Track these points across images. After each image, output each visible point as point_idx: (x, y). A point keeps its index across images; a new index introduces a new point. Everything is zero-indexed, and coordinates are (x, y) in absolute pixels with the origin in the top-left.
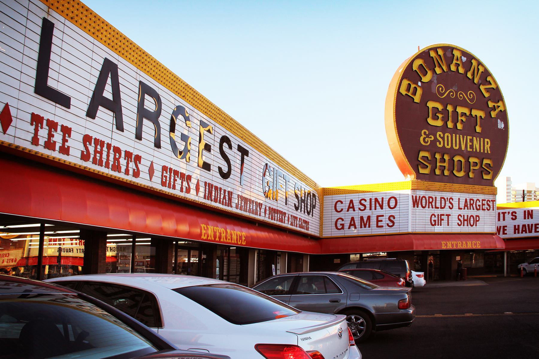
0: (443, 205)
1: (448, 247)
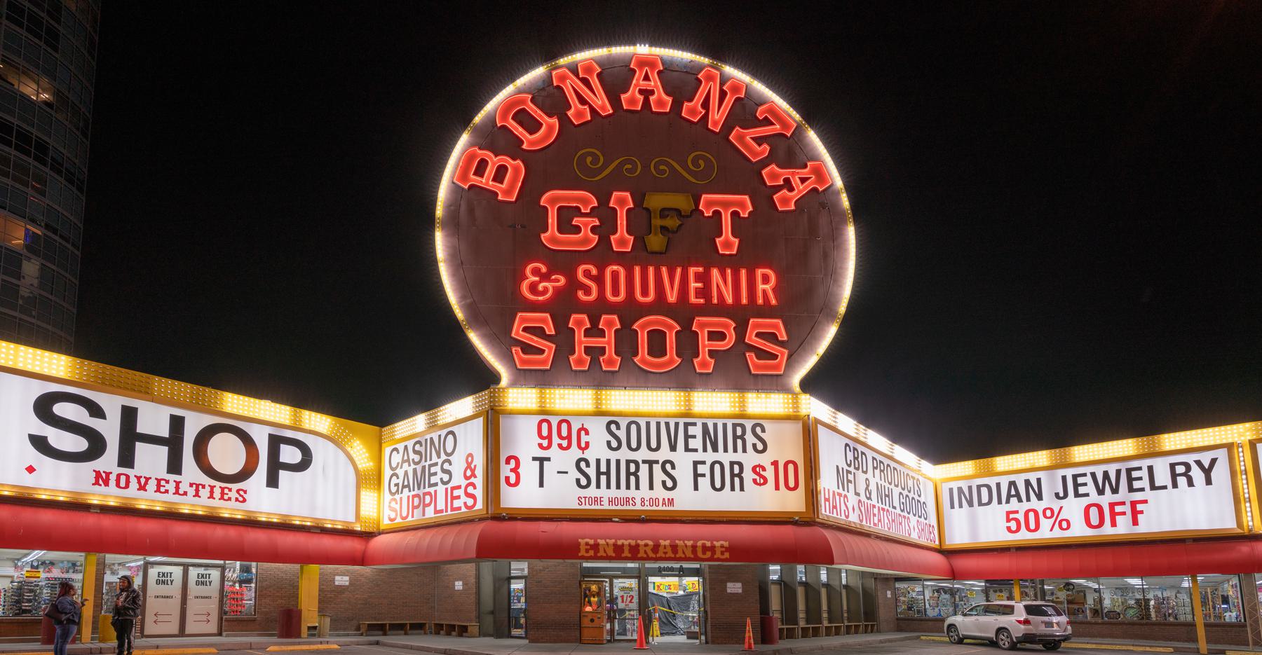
1: (850, 519)
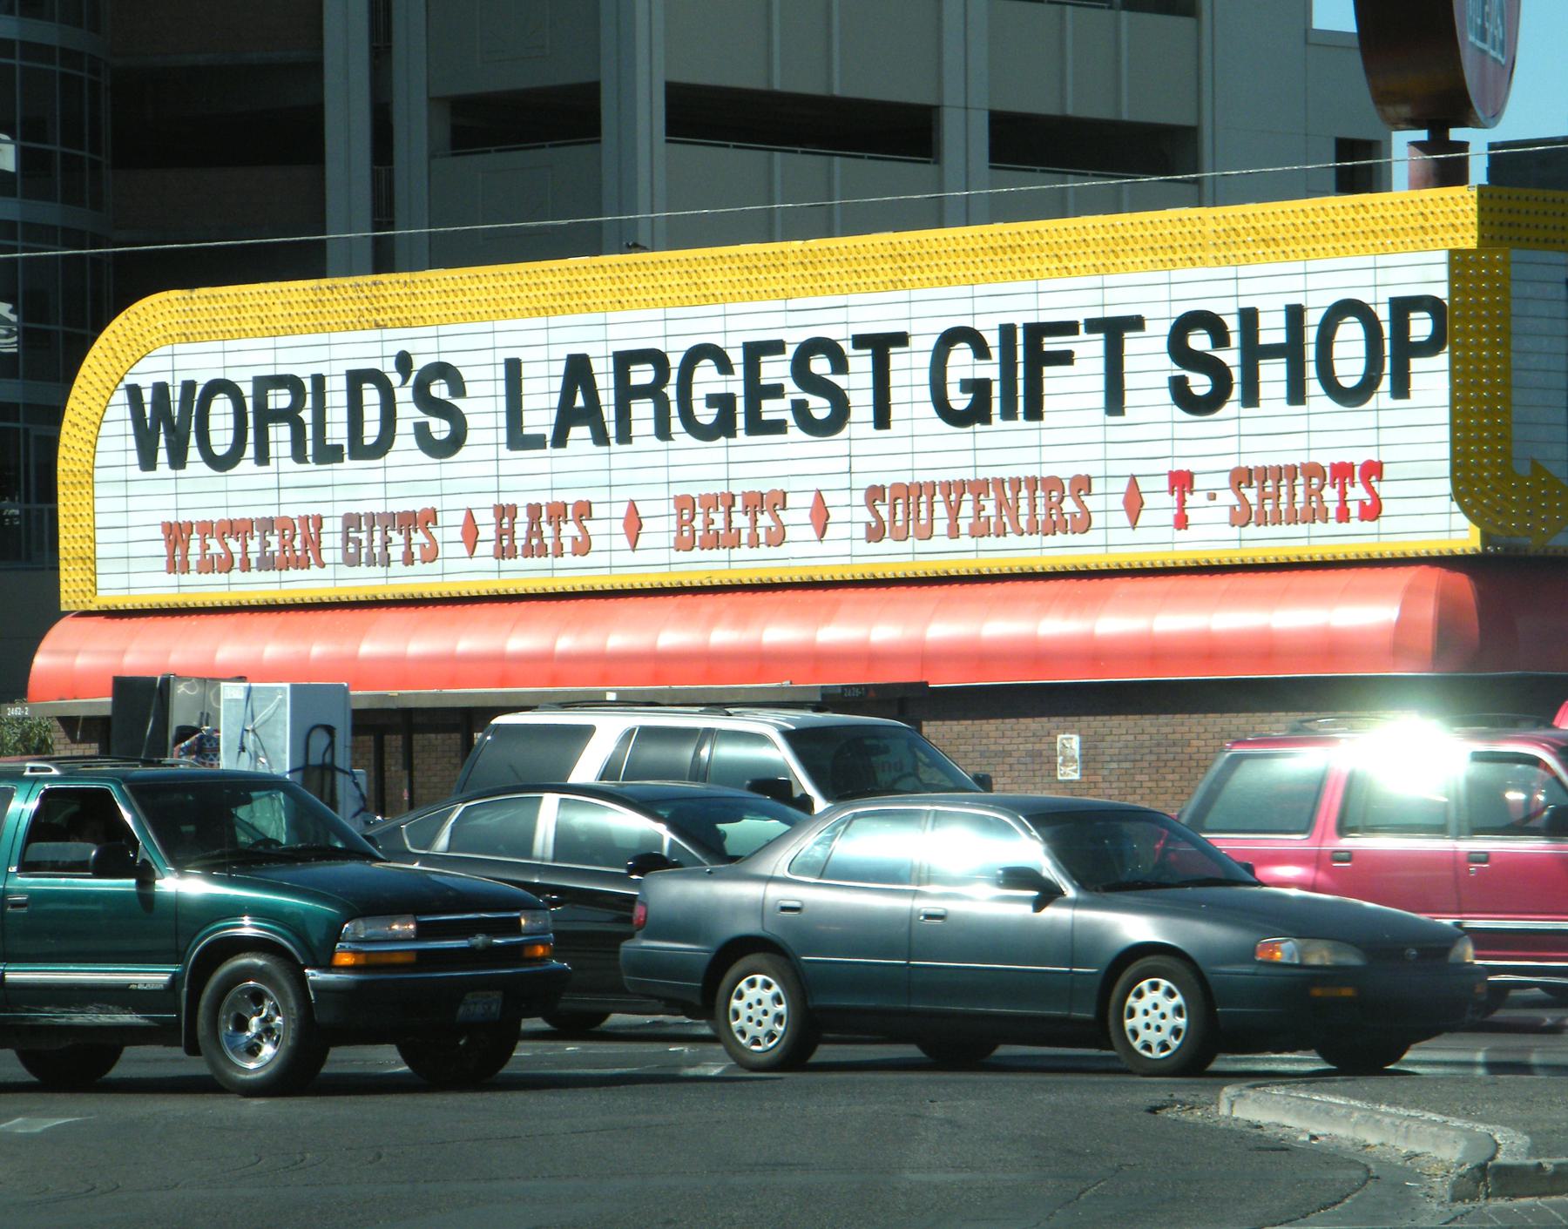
0: (371, 432)
